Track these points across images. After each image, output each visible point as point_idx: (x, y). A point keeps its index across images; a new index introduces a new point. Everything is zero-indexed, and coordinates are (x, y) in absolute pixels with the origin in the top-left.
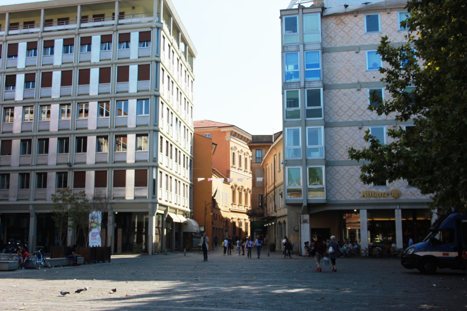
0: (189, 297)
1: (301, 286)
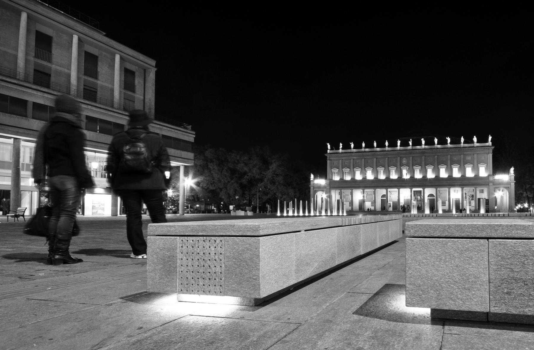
0: (60, 113)
1: (345, 186)
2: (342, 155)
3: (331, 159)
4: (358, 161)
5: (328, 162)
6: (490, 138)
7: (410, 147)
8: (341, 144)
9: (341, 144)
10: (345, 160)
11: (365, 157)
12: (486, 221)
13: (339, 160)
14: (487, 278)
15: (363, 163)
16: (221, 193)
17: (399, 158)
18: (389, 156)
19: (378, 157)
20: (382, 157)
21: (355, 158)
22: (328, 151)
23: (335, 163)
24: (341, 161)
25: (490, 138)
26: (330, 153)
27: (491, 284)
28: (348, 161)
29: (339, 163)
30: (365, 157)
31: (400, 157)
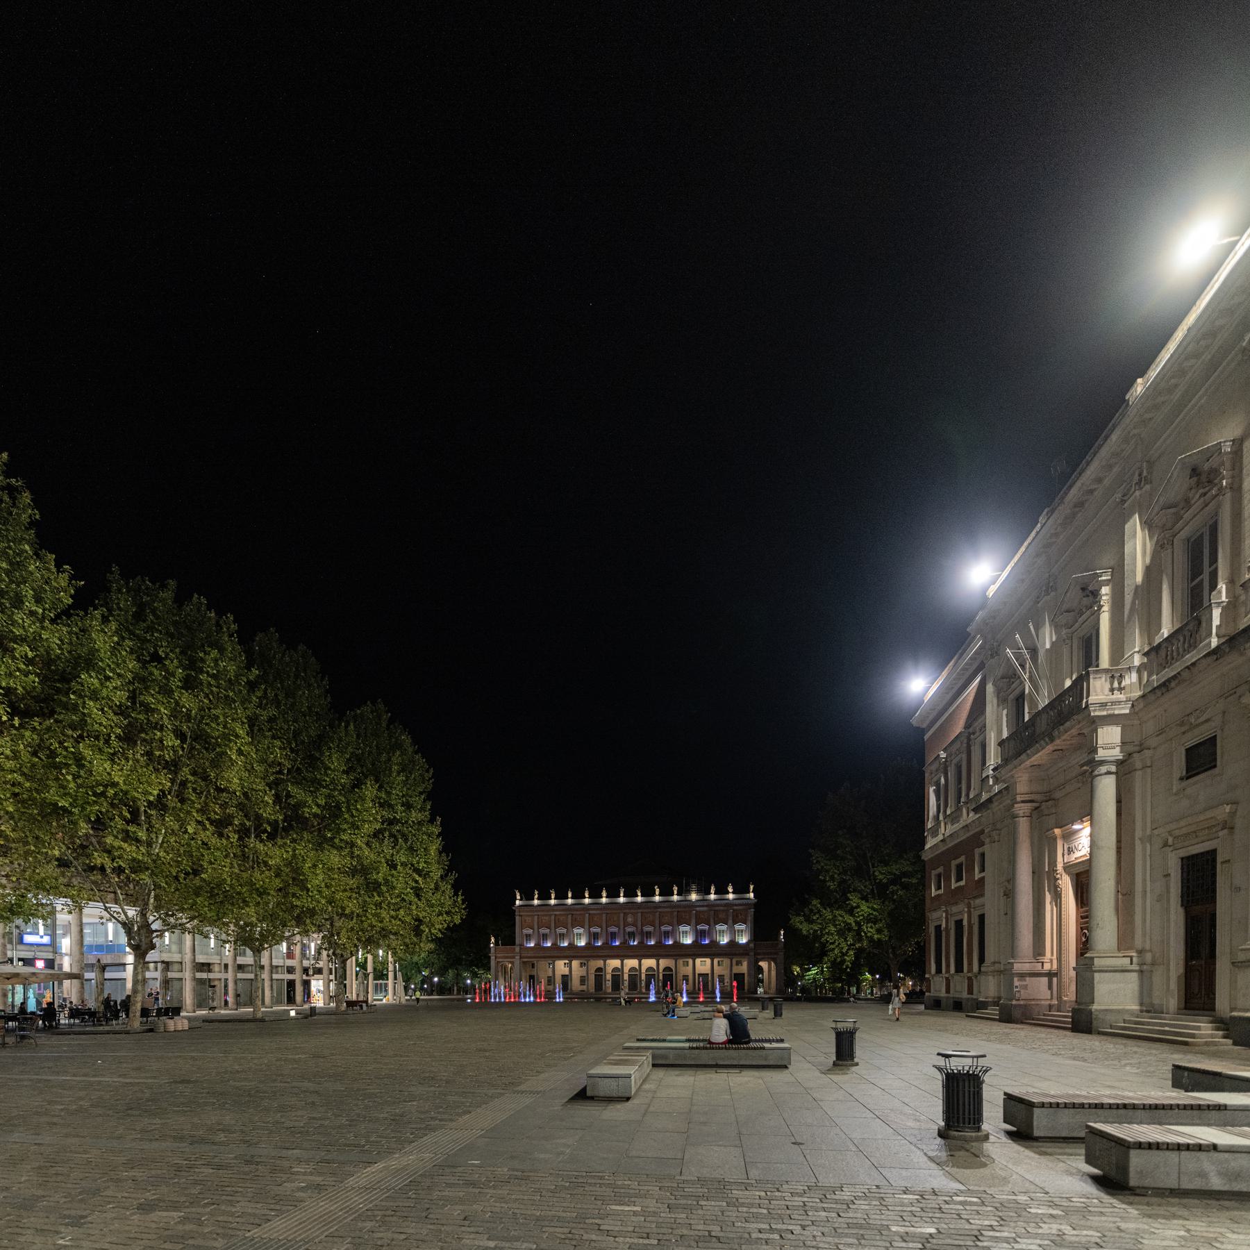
1: (559, 955)
2: (555, 908)
3: (521, 914)
4: (527, 918)
5: (517, 918)
6: (752, 887)
7: (553, 902)
8: (536, 892)
9: (536, 892)
10: (543, 915)
11: (591, 912)
12: (1206, 1162)
13: (534, 916)
14: (275, 950)
15: (570, 921)
16: (835, 1059)
17: (622, 915)
18: (608, 912)
19: (575, 913)
20: (598, 912)
21: (557, 913)
22: (518, 902)
23: (528, 919)
24: (536, 917)
25: (752, 887)
26: (520, 906)
27: (679, 1156)
28: (547, 918)
29: (533, 921)
30: (591, 912)
31: (624, 913)
